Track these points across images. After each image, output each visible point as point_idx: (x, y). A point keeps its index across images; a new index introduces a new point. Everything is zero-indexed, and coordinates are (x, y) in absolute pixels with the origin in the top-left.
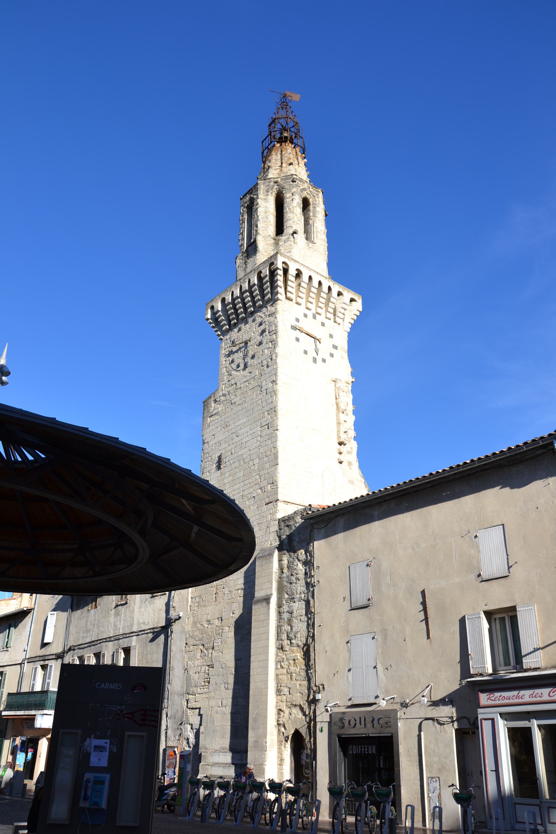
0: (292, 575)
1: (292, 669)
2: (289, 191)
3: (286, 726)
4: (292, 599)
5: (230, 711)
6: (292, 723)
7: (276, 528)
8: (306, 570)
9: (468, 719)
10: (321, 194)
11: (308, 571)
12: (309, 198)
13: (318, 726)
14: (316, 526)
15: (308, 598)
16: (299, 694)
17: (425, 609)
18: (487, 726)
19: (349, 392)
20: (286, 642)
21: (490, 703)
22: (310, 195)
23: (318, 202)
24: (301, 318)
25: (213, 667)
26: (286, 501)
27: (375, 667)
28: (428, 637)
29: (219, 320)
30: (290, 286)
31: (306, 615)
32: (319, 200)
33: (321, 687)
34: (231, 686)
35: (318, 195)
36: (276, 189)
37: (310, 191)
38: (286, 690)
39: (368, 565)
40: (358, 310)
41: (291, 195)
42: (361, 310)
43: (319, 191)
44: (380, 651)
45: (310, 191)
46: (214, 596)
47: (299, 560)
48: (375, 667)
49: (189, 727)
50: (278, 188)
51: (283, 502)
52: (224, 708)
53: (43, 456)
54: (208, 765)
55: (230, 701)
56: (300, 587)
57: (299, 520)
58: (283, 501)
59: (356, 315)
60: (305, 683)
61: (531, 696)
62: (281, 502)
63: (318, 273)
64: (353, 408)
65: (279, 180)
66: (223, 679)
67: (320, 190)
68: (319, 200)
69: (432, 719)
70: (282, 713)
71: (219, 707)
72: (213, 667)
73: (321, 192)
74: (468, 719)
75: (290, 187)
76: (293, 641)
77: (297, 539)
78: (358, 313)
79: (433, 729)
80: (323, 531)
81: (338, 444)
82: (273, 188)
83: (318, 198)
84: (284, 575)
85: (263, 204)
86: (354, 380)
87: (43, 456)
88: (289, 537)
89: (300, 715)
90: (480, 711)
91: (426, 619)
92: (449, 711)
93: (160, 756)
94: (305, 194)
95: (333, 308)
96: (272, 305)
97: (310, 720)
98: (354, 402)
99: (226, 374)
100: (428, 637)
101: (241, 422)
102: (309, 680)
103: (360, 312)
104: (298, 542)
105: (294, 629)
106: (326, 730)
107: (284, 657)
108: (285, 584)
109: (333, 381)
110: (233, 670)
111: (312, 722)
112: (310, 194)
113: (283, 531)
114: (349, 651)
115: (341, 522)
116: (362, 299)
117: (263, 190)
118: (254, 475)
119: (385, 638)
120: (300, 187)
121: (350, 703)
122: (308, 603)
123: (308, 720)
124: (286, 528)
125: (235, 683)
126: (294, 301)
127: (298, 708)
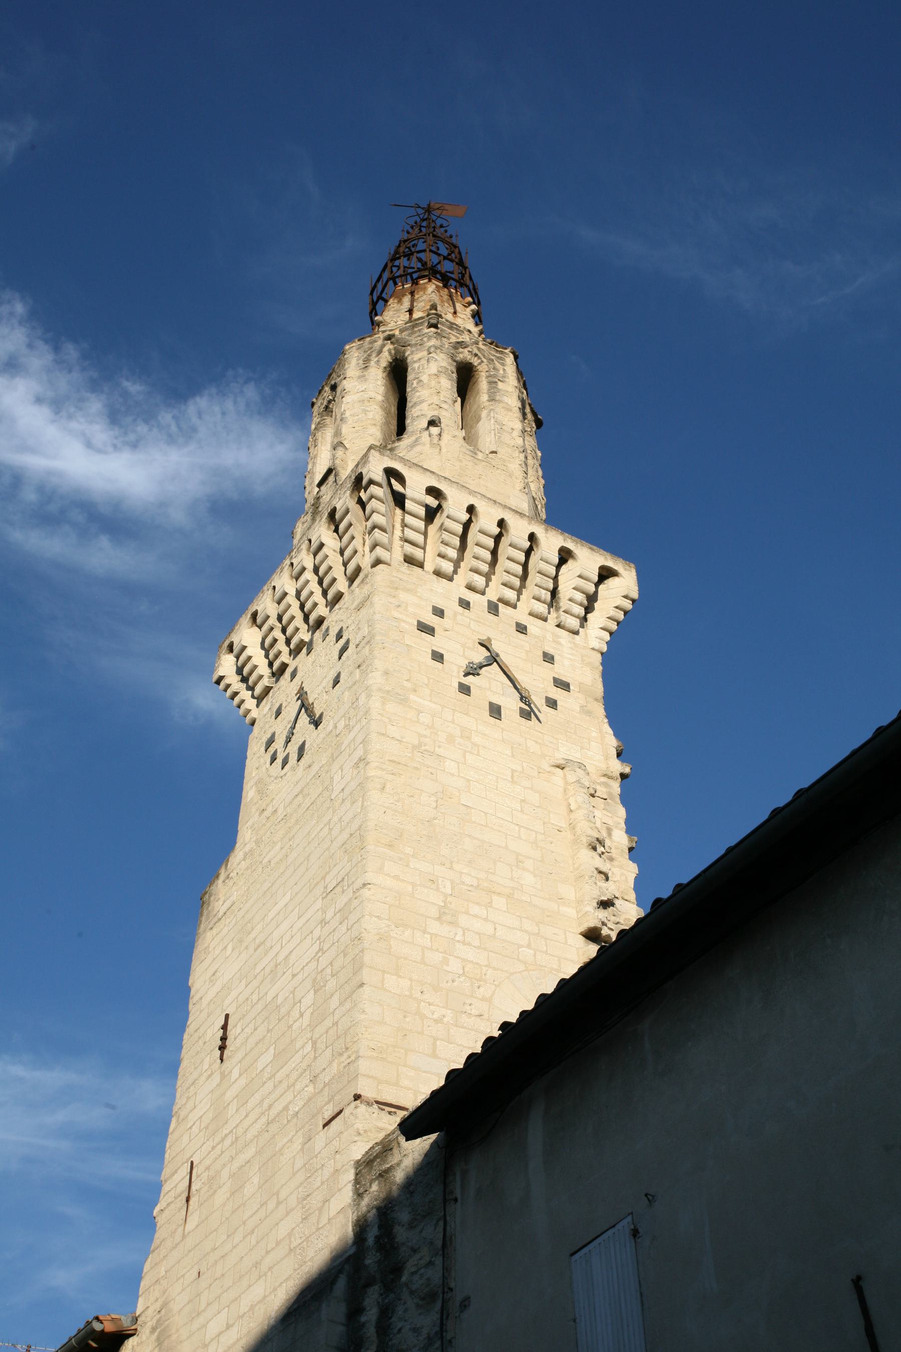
2: (419, 347)
10: (510, 359)
12: (476, 364)
19: (612, 798)
22: (479, 358)
23: (501, 372)
24: (451, 607)
26: (389, 1102)
30: (411, 529)
32: (504, 370)
35: (503, 359)
36: (389, 351)
37: (479, 349)
40: (626, 597)
41: (425, 353)
42: (635, 595)
43: (505, 353)
45: (479, 349)
50: (395, 349)
51: (375, 1106)
53: (94, 1345)
58: (377, 1102)
59: (621, 609)
62: (369, 1104)
63: (495, 501)
64: (631, 841)
65: (397, 332)
67: (507, 351)
68: (504, 370)
73: (512, 356)
75: (422, 340)
77: (404, 1216)
78: (628, 605)
81: (582, 939)
82: (380, 352)
83: (503, 365)
85: (355, 386)
86: (627, 770)
87: (94, 1345)
94: (464, 355)
95: (547, 590)
98: (631, 827)
101: (281, 904)
103: (633, 601)
104: (411, 1226)
109: (558, 767)
112: (480, 355)
116: (637, 572)
117: (358, 360)
118: (298, 1045)
120: (449, 338)
126: (429, 566)
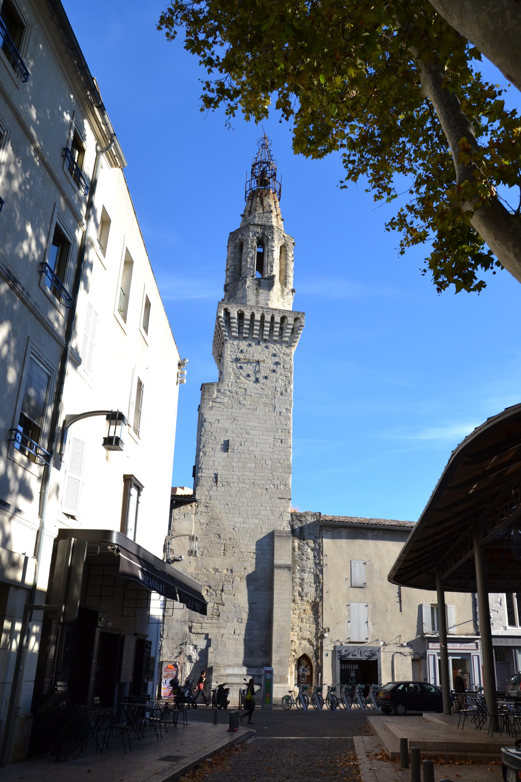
0: (303, 554)
1: (303, 616)
3: (297, 651)
4: (303, 571)
5: (243, 638)
6: (302, 650)
7: (289, 518)
8: (314, 554)
9: (419, 654)
11: (316, 555)
13: (324, 653)
14: (324, 528)
15: (316, 573)
16: (308, 632)
17: (400, 596)
18: (431, 658)
20: (298, 598)
21: (433, 647)
25: (224, 605)
27: (367, 622)
28: (401, 611)
29: (232, 320)
31: (315, 583)
33: (327, 630)
34: (245, 621)
38: (298, 628)
39: (364, 564)
44: (370, 613)
46: (223, 551)
47: (309, 546)
48: (367, 622)
49: (192, 647)
52: (237, 636)
54: (223, 676)
55: (243, 632)
56: (310, 564)
57: (310, 520)
60: (314, 626)
61: (452, 646)
66: (236, 615)
69: (401, 653)
70: (293, 643)
71: (231, 635)
72: (224, 605)
74: (419, 654)
76: (305, 598)
79: (400, 658)
80: (330, 533)
84: (296, 553)
88: (301, 528)
89: (308, 646)
90: (428, 651)
91: (400, 601)
92: (408, 650)
93: (125, 656)
96: (287, 347)
97: (318, 648)
99: (233, 374)
100: (401, 611)
102: (317, 624)
105: (305, 591)
106: (330, 655)
107: (296, 607)
108: (297, 559)
110: (248, 610)
111: (319, 651)
113: (295, 522)
114: (349, 611)
115: (344, 532)
119: (374, 607)
121: (348, 641)
122: (316, 576)
123: (315, 649)
124: (297, 521)
125: (249, 620)
127: (306, 641)
